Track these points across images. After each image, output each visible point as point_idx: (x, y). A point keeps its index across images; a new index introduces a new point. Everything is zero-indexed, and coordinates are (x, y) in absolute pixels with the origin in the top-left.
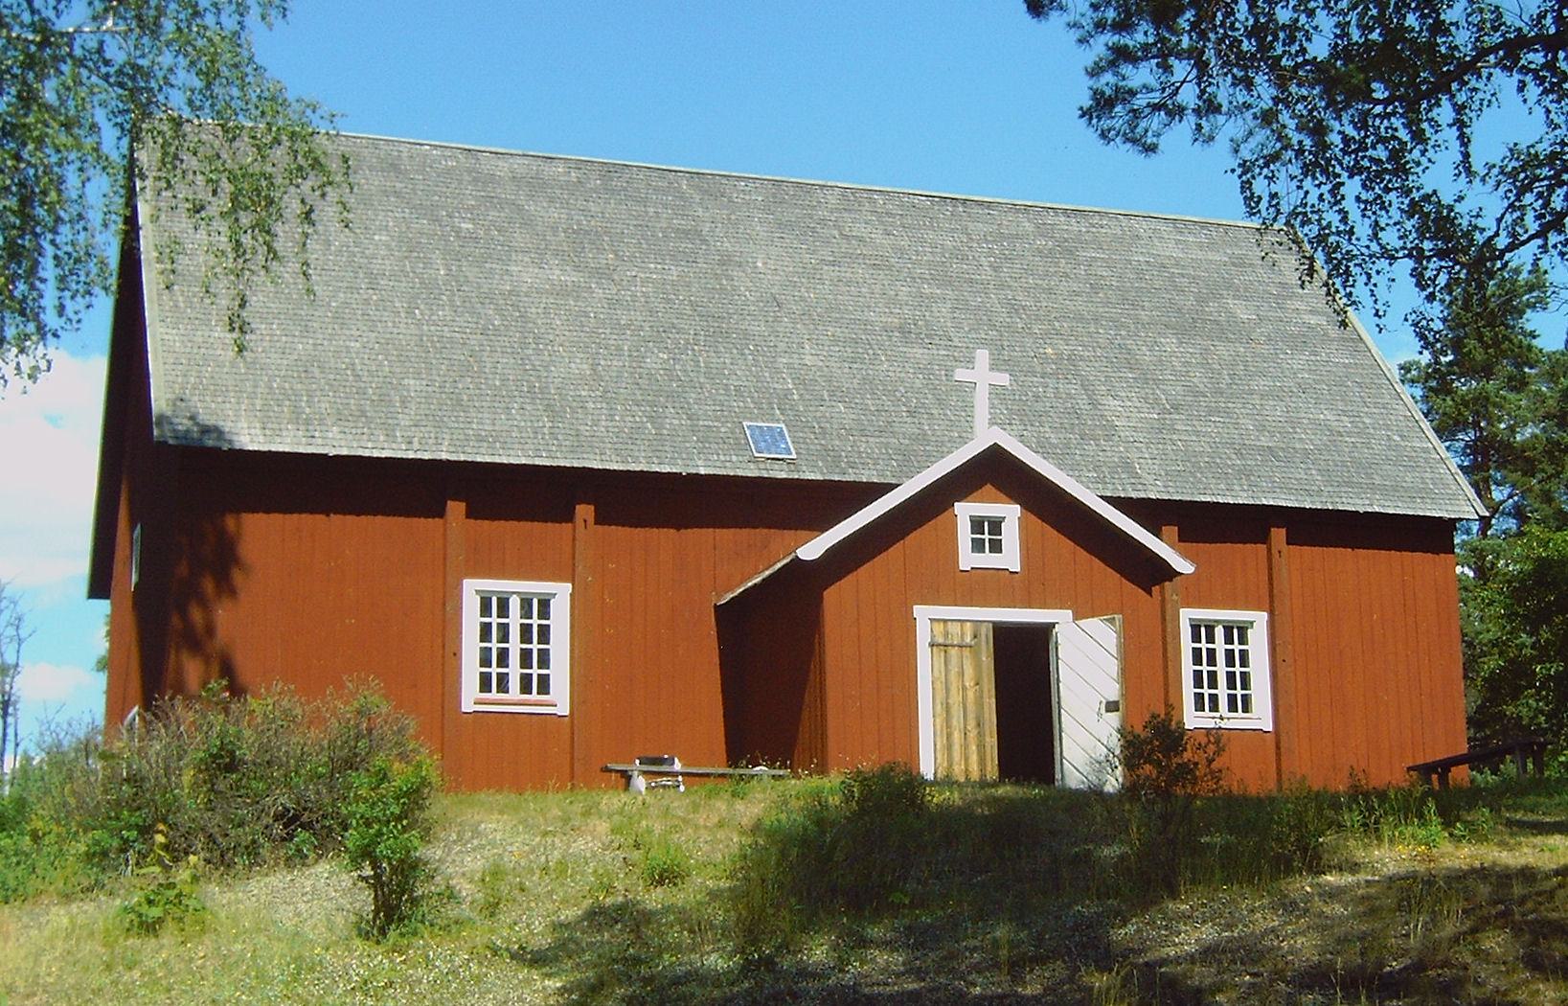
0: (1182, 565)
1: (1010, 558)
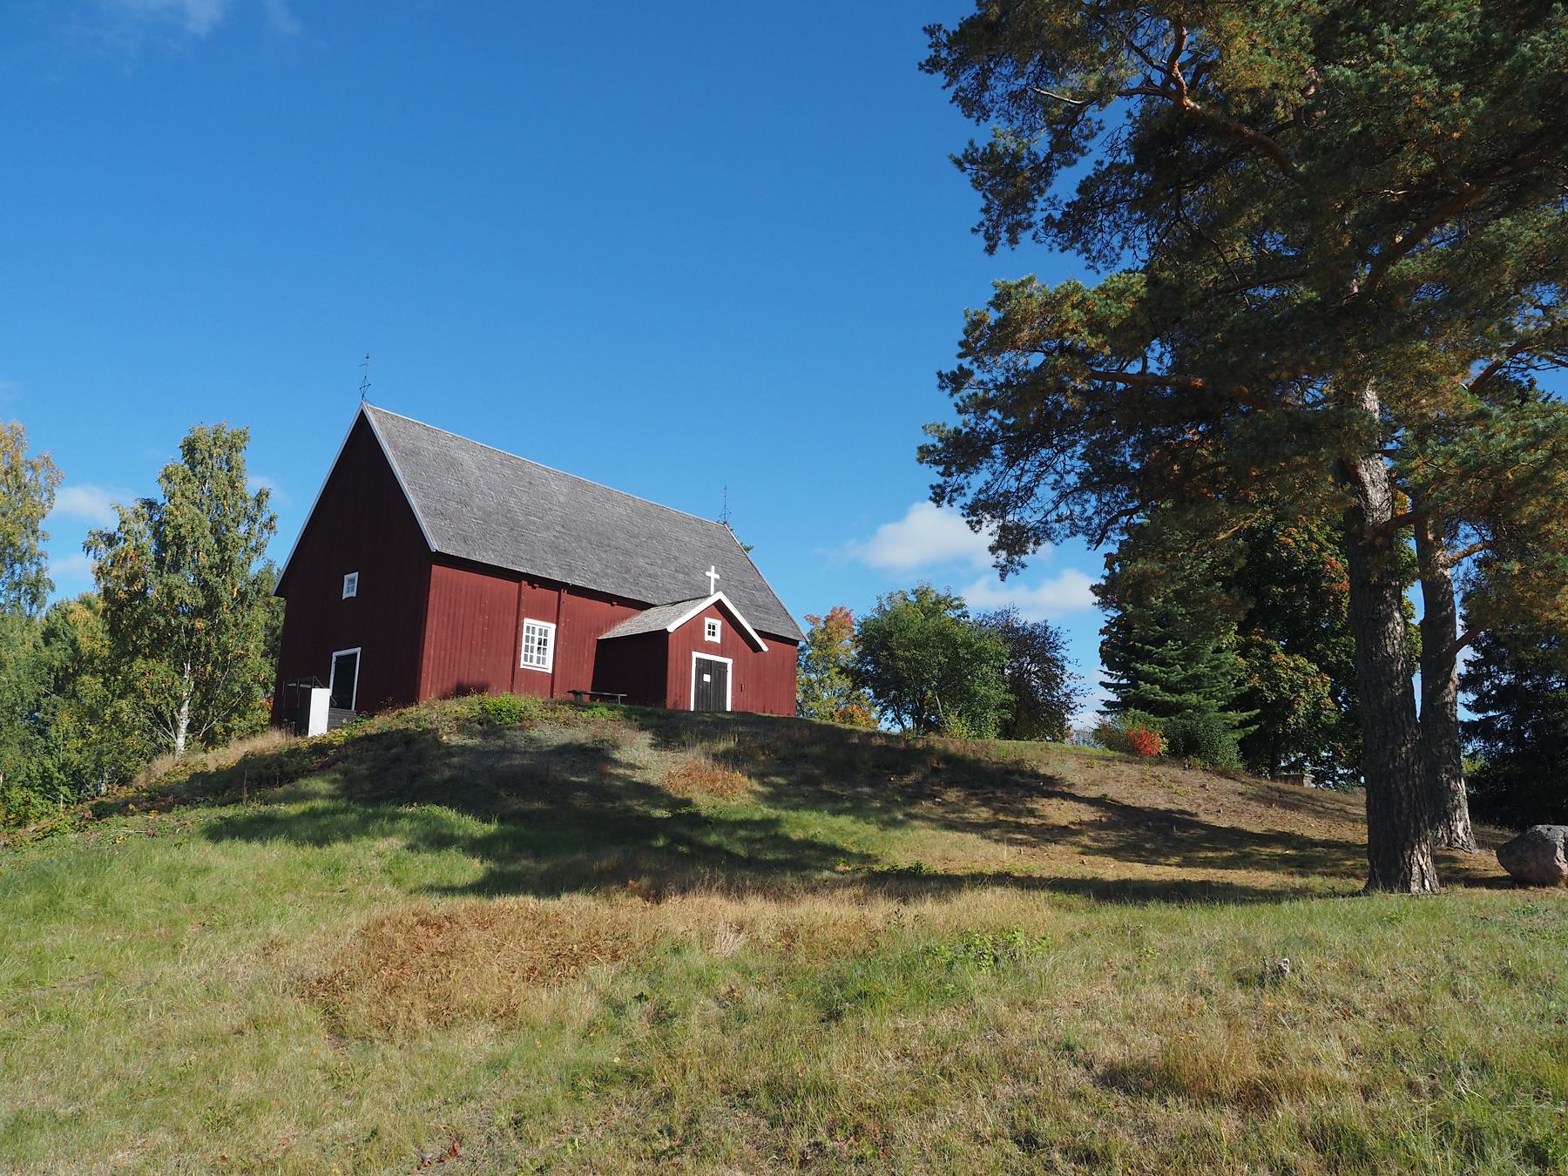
0: (765, 648)
1: (717, 639)
